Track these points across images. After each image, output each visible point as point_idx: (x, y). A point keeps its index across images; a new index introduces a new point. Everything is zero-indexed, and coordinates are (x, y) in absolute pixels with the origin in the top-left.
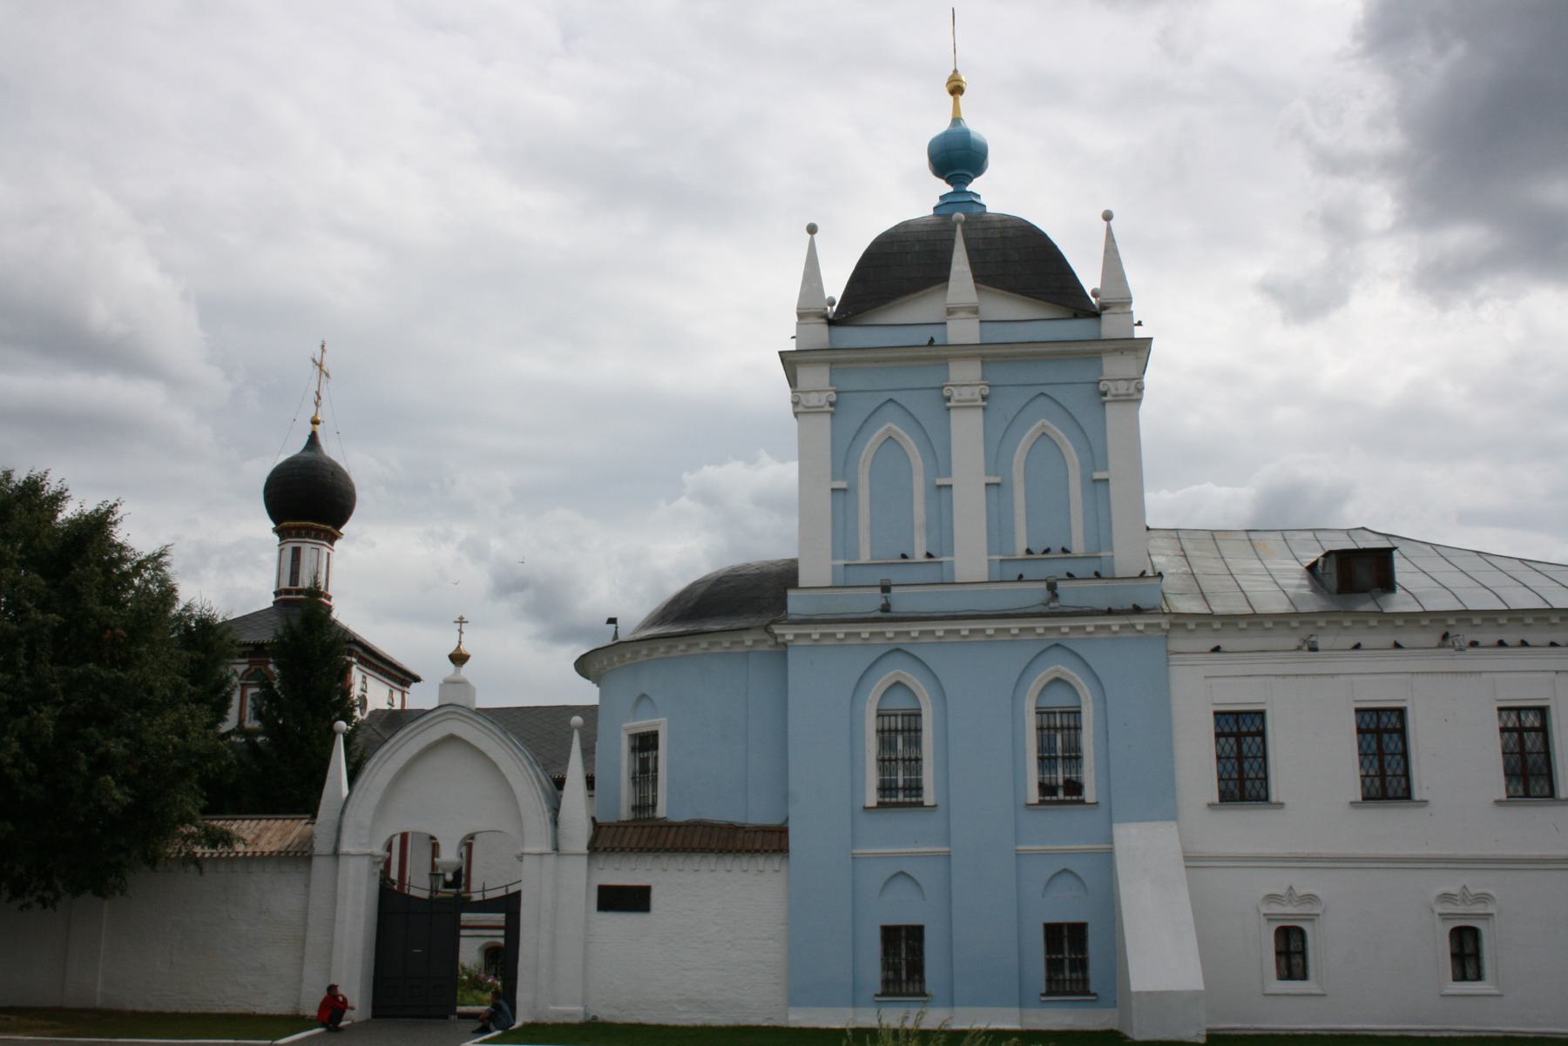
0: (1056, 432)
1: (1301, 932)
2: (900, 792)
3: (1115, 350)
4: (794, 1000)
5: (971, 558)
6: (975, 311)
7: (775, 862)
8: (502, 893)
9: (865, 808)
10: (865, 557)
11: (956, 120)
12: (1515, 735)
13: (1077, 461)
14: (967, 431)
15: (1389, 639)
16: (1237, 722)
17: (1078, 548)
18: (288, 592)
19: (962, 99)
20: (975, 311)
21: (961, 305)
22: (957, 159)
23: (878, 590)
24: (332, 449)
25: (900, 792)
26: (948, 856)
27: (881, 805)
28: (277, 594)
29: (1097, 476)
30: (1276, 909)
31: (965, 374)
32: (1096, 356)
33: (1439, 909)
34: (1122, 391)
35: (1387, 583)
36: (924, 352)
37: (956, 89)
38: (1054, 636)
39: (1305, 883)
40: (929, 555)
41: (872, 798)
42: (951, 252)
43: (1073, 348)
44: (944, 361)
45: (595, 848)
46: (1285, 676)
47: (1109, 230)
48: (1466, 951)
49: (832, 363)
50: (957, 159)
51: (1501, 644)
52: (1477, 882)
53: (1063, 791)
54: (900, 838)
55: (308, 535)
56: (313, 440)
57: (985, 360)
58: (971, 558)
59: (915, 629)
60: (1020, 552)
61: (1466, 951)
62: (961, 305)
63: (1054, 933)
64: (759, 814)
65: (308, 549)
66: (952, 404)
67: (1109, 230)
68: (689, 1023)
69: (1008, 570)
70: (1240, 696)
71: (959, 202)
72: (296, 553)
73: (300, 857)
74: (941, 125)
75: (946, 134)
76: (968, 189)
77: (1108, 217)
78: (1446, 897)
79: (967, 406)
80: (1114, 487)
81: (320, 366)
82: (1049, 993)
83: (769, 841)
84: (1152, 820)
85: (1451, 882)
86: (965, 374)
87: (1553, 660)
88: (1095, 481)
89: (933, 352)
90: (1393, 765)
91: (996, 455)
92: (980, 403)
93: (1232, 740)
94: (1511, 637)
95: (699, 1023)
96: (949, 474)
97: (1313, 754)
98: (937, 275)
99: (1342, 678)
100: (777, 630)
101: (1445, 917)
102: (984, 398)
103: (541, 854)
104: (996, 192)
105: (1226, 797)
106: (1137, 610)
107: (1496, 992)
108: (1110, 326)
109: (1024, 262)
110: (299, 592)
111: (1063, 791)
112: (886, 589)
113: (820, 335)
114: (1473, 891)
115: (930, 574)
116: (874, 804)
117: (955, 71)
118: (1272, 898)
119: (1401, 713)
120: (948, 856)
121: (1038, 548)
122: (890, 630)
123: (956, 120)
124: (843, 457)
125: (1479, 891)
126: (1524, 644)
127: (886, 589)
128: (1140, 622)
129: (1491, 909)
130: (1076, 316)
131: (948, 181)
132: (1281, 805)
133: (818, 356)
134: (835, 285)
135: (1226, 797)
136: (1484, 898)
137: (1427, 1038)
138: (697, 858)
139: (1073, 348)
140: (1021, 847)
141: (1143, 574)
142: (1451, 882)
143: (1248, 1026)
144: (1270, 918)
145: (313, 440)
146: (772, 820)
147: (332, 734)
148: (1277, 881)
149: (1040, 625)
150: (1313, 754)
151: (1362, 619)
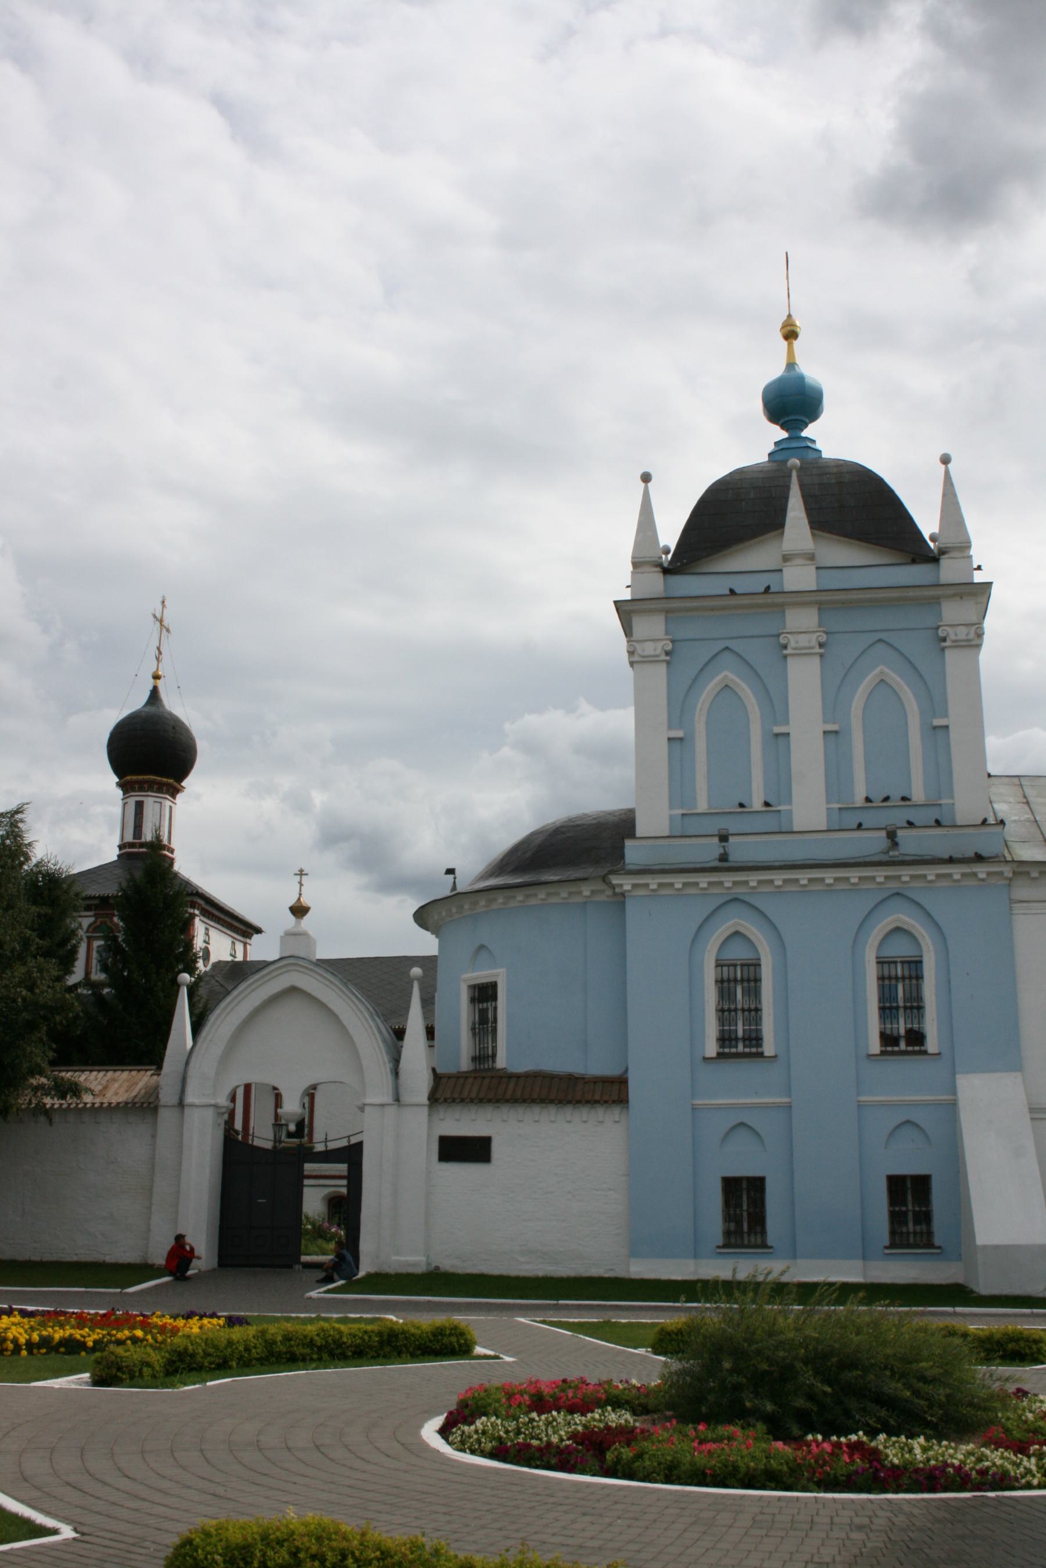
2: (740, 1042)
4: (635, 1251)
5: (809, 807)
6: (811, 557)
7: (616, 1112)
8: (344, 1143)
11: (791, 365)
14: (804, 678)
17: (918, 795)
18: (131, 845)
19: (796, 344)
20: (811, 557)
21: (797, 553)
22: (792, 404)
23: (716, 840)
24: (175, 705)
25: (740, 1042)
26: (789, 1107)
27: (720, 1056)
28: (120, 847)
29: (937, 722)
31: (802, 621)
38: (894, 885)
40: (767, 804)
41: (711, 1049)
42: (786, 498)
43: (911, 593)
44: (781, 608)
45: (436, 1099)
49: (667, 611)
50: (792, 404)
53: (904, 1041)
54: (740, 1089)
55: (150, 789)
56: (154, 695)
58: (809, 807)
59: (753, 878)
62: (797, 553)
63: (731, 1186)
64: (598, 1066)
65: (151, 803)
66: (947, 644)
69: (847, 818)
71: (794, 447)
72: (139, 806)
73: (146, 1107)
75: (780, 381)
76: (804, 434)
77: (946, 460)
79: (803, 653)
82: (893, 1245)
83: (609, 1091)
86: (802, 621)
88: (935, 728)
89: (733, 601)
91: (834, 703)
92: (663, 657)
98: (771, 521)
100: (615, 880)
102: (821, 645)
103: (382, 1105)
104: (832, 437)
106: (979, 858)
108: (948, 571)
109: (861, 507)
110: (142, 845)
111: (904, 1041)
112: (724, 838)
113: (655, 584)
115: (768, 823)
116: (714, 1055)
117: (789, 316)
120: (789, 1107)
122: (728, 879)
123: (791, 365)
124: (679, 708)
127: (724, 838)
128: (982, 870)
130: (914, 561)
134: (669, 533)
138: (536, 1109)
139: (911, 593)
140: (862, 1098)
141: (984, 822)
145: (154, 695)
147: (176, 986)
149: (880, 874)
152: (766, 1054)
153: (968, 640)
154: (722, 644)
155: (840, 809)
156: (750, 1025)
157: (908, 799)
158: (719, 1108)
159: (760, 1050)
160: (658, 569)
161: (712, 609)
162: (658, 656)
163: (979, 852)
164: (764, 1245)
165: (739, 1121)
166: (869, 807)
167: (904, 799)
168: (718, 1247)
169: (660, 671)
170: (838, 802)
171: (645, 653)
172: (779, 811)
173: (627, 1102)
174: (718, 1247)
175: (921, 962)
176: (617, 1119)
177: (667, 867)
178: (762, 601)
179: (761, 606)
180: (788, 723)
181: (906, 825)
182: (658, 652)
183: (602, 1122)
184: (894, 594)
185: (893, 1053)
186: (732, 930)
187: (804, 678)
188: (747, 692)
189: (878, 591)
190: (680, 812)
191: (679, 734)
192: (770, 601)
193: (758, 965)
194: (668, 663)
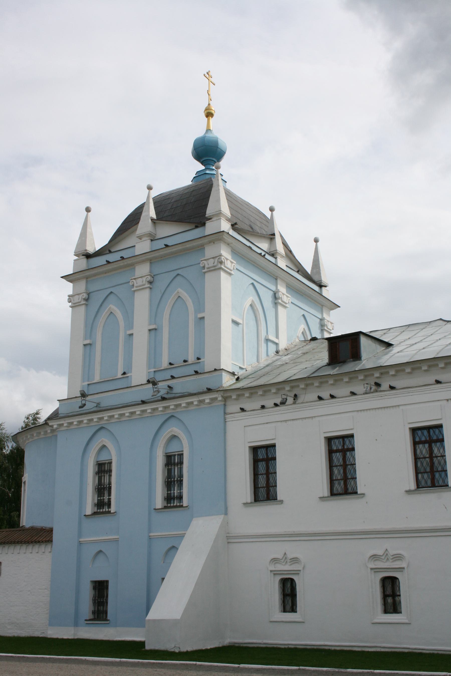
0: (119, 314)
1: (292, 580)
2: (102, 505)
3: (210, 242)
4: (51, 624)
5: (139, 375)
9: (85, 515)
10: (97, 379)
12: (427, 445)
13: (193, 309)
14: (142, 300)
15: (346, 391)
16: (429, 432)
30: (280, 567)
32: (201, 248)
33: (372, 565)
34: (211, 265)
35: (356, 355)
36: (122, 263)
37: (209, 114)
39: (293, 550)
43: (188, 245)
44: (132, 266)
46: (286, 421)
47: (316, 245)
48: (391, 593)
49: (87, 278)
51: (353, 394)
52: (393, 546)
53: (173, 500)
54: (100, 531)
57: (151, 261)
60: (165, 364)
61: (391, 593)
67: (316, 245)
68: (11, 635)
70: (261, 437)
74: (200, 133)
78: (374, 557)
80: (206, 321)
81: (87, 300)
84: (212, 515)
85: (378, 547)
86: (143, 270)
87: (440, 393)
90: (262, 481)
91: (155, 312)
92: (83, 302)
93: (427, 445)
94: (325, 395)
95: (16, 635)
96: (132, 328)
97: (302, 469)
99: (317, 419)
101: (375, 570)
105: (257, 499)
106: (209, 390)
107: (407, 621)
111: (173, 500)
113: (83, 263)
114: (392, 552)
118: (275, 560)
119: (329, 440)
121: (178, 361)
122: (95, 417)
123: (208, 130)
124: (90, 328)
125: (395, 552)
126: (332, 397)
128: (207, 398)
129: (404, 565)
130: (197, 227)
131: (202, 163)
132: (282, 502)
133: (144, 258)
135: (257, 499)
136: (398, 557)
137: (363, 652)
139: (188, 245)
142: (378, 547)
143: (259, 641)
144: (275, 573)
146: (46, 524)
148: (277, 550)
150: (302, 469)
151: (353, 376)
152: (184, 506)
153: (214, 266)
154: (174, 274)
155: (155, 371)
156: (101, 497)
157: (173, 364)
158: (161, 537)
159: (181, 504)
160: (84, 257)
161: (106, 272)
162: (80, 302)
163: (209, 387)
164: (106, 619)
165: (171, 546)
166: (186, 365)
167: (185, 361)
168: (86, 620)
169: (82, 309)
170: (154, 368)
171: (75, 302)
172: (128, 377)
173: (52, 541)
174: (86, 620)
175: (182, 454)
176: (43, 551)
177: (75, 413)
178: (122, 264)
179: (121, 268)
180: (204, 311)
181: (194, 373)
182: (144, 283)
183: (44, 552)
184: (180, 247)
185: (171, 507)
186: (101, 445)
187: (142, 300)
188: (119, 314)
189: (186, 244)
190: (86, 383)
191: (87, 342)
192: (126, 263)
193: (110, 463)
194: (86, 305)
